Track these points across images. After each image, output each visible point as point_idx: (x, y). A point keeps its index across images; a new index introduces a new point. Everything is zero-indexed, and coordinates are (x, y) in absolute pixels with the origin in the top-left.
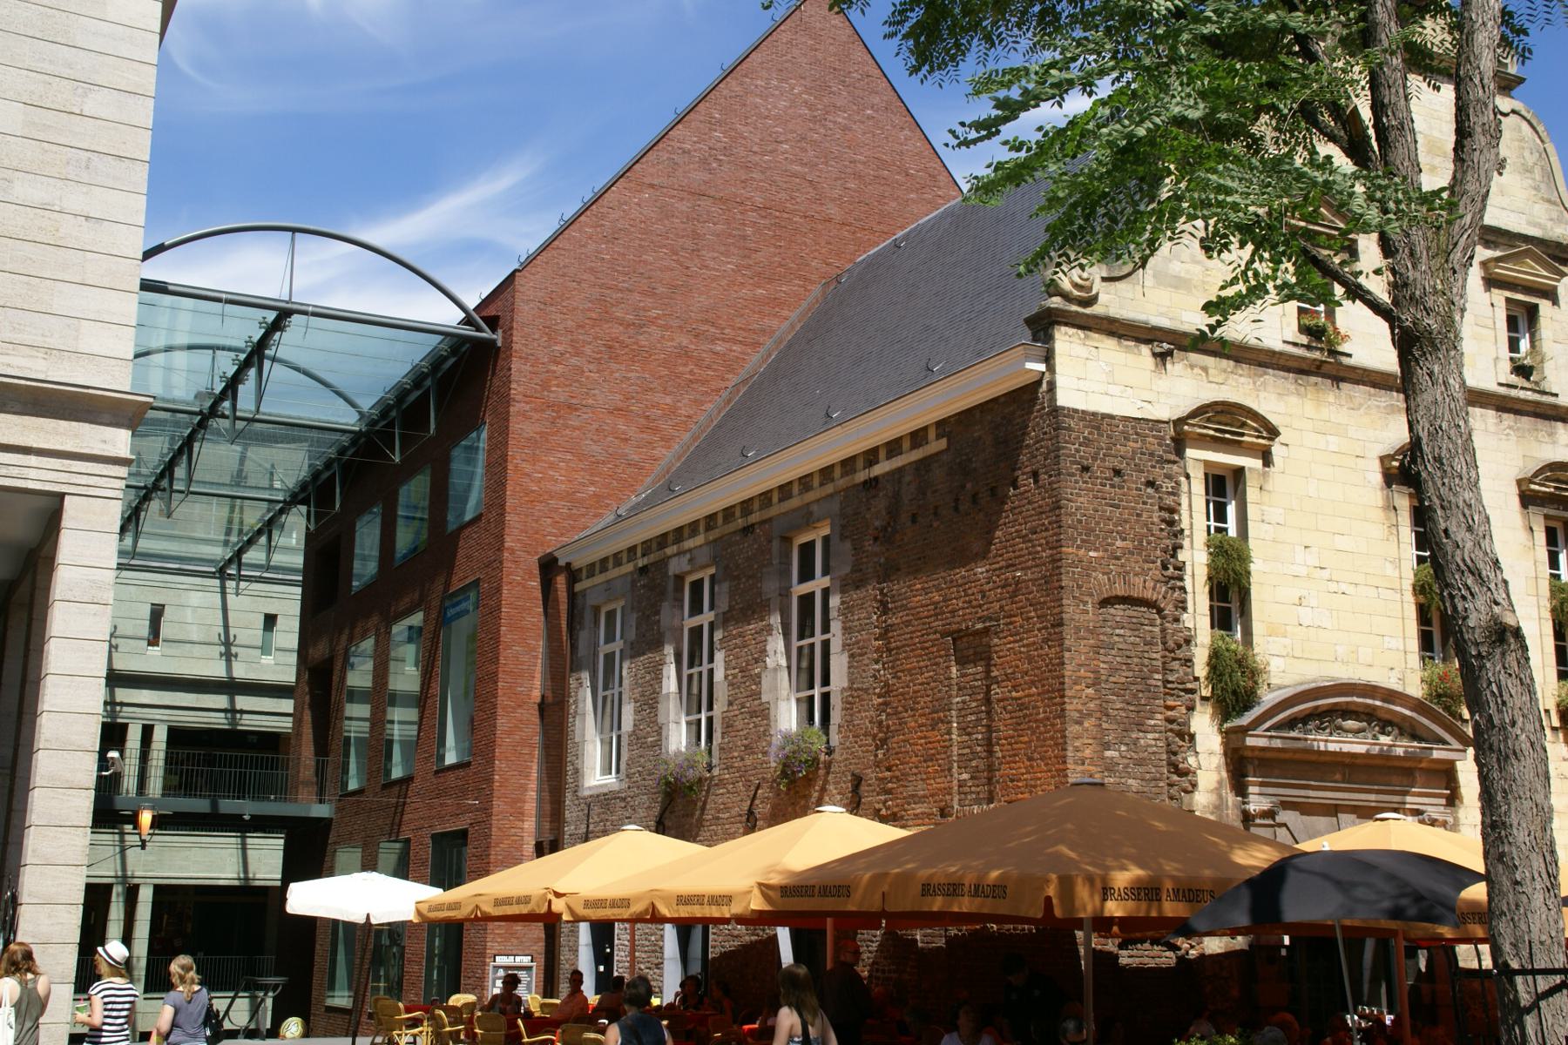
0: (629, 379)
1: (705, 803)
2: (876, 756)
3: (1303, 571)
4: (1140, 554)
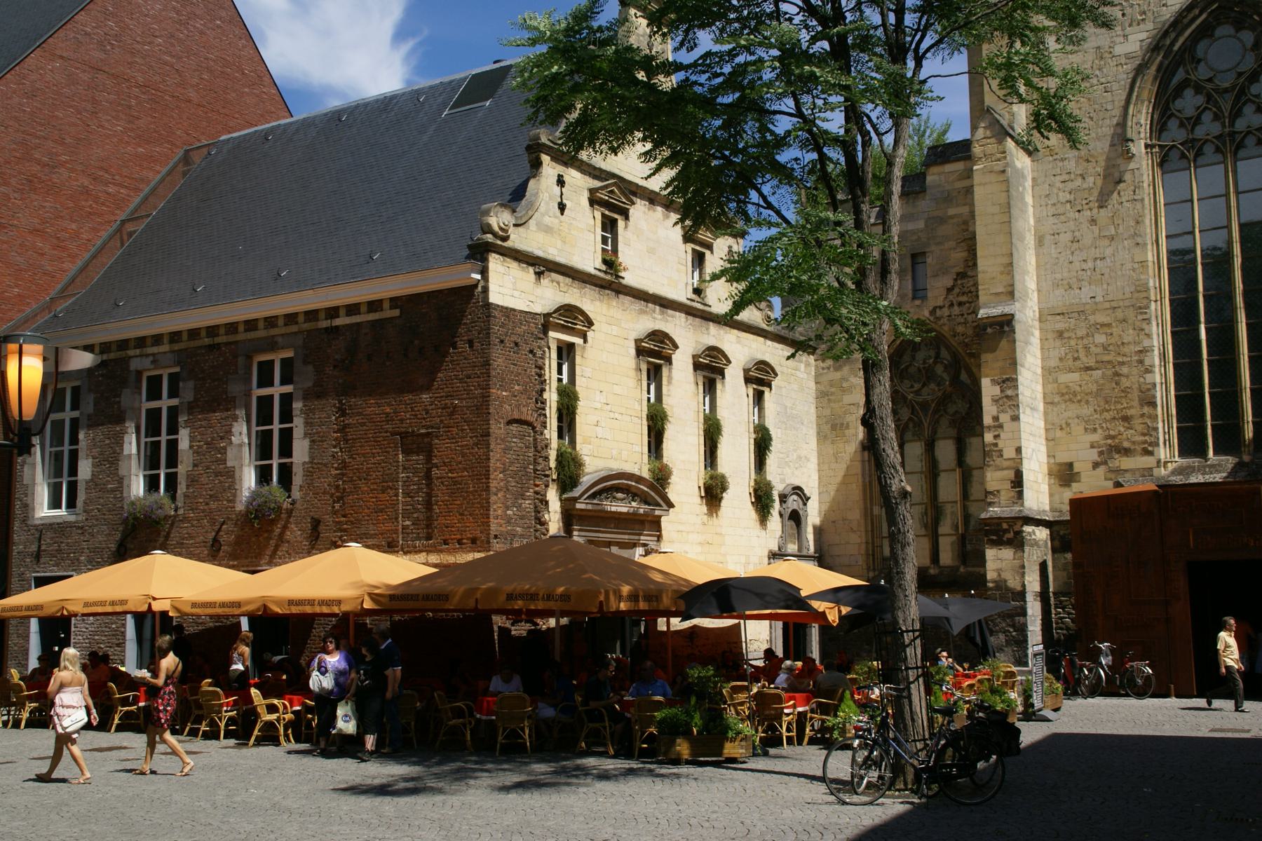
0: (44, 207)
1: (169, 533)
2: (334, 507)
3: (598, 406)
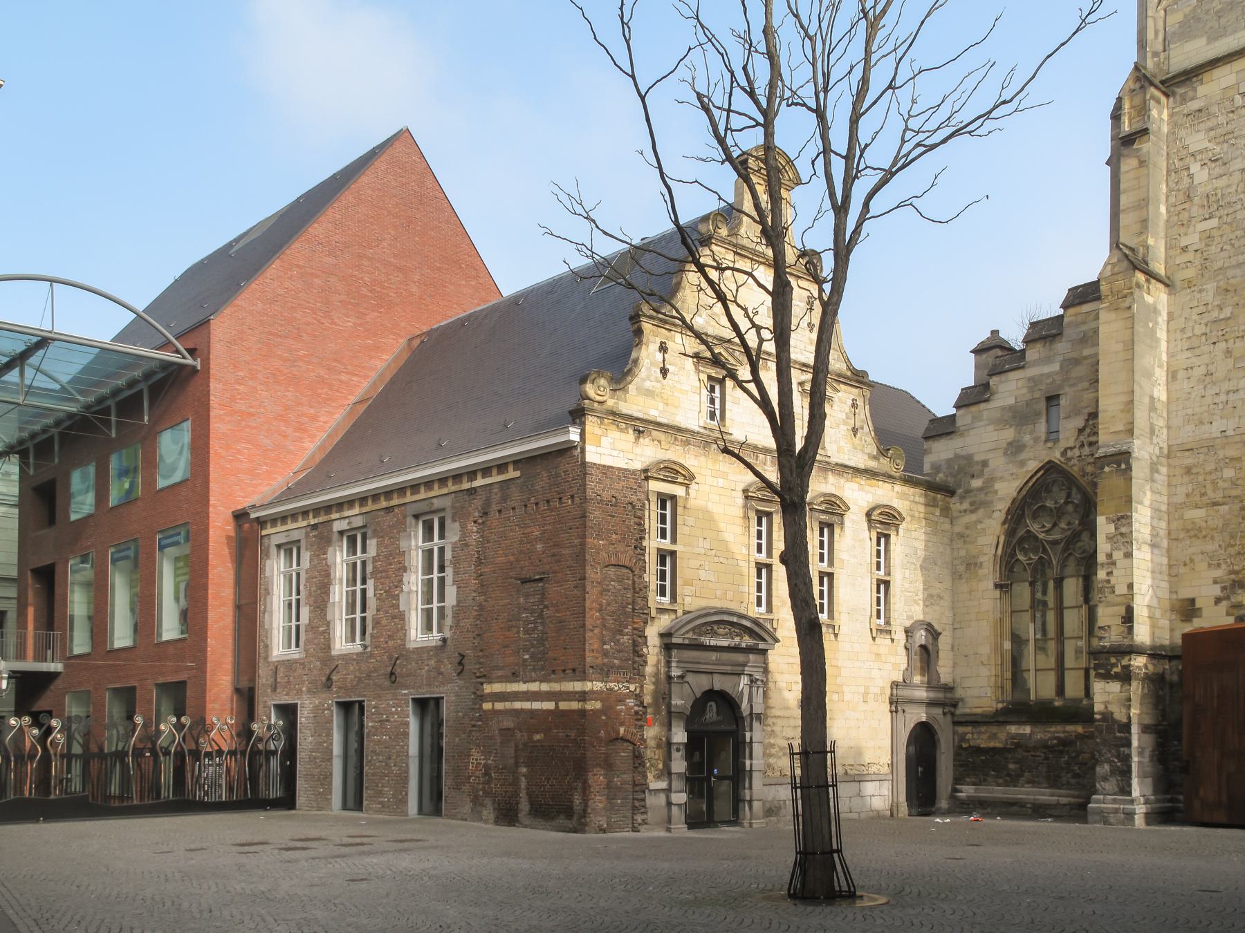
3: (702, 551)
4: (624, 542)
